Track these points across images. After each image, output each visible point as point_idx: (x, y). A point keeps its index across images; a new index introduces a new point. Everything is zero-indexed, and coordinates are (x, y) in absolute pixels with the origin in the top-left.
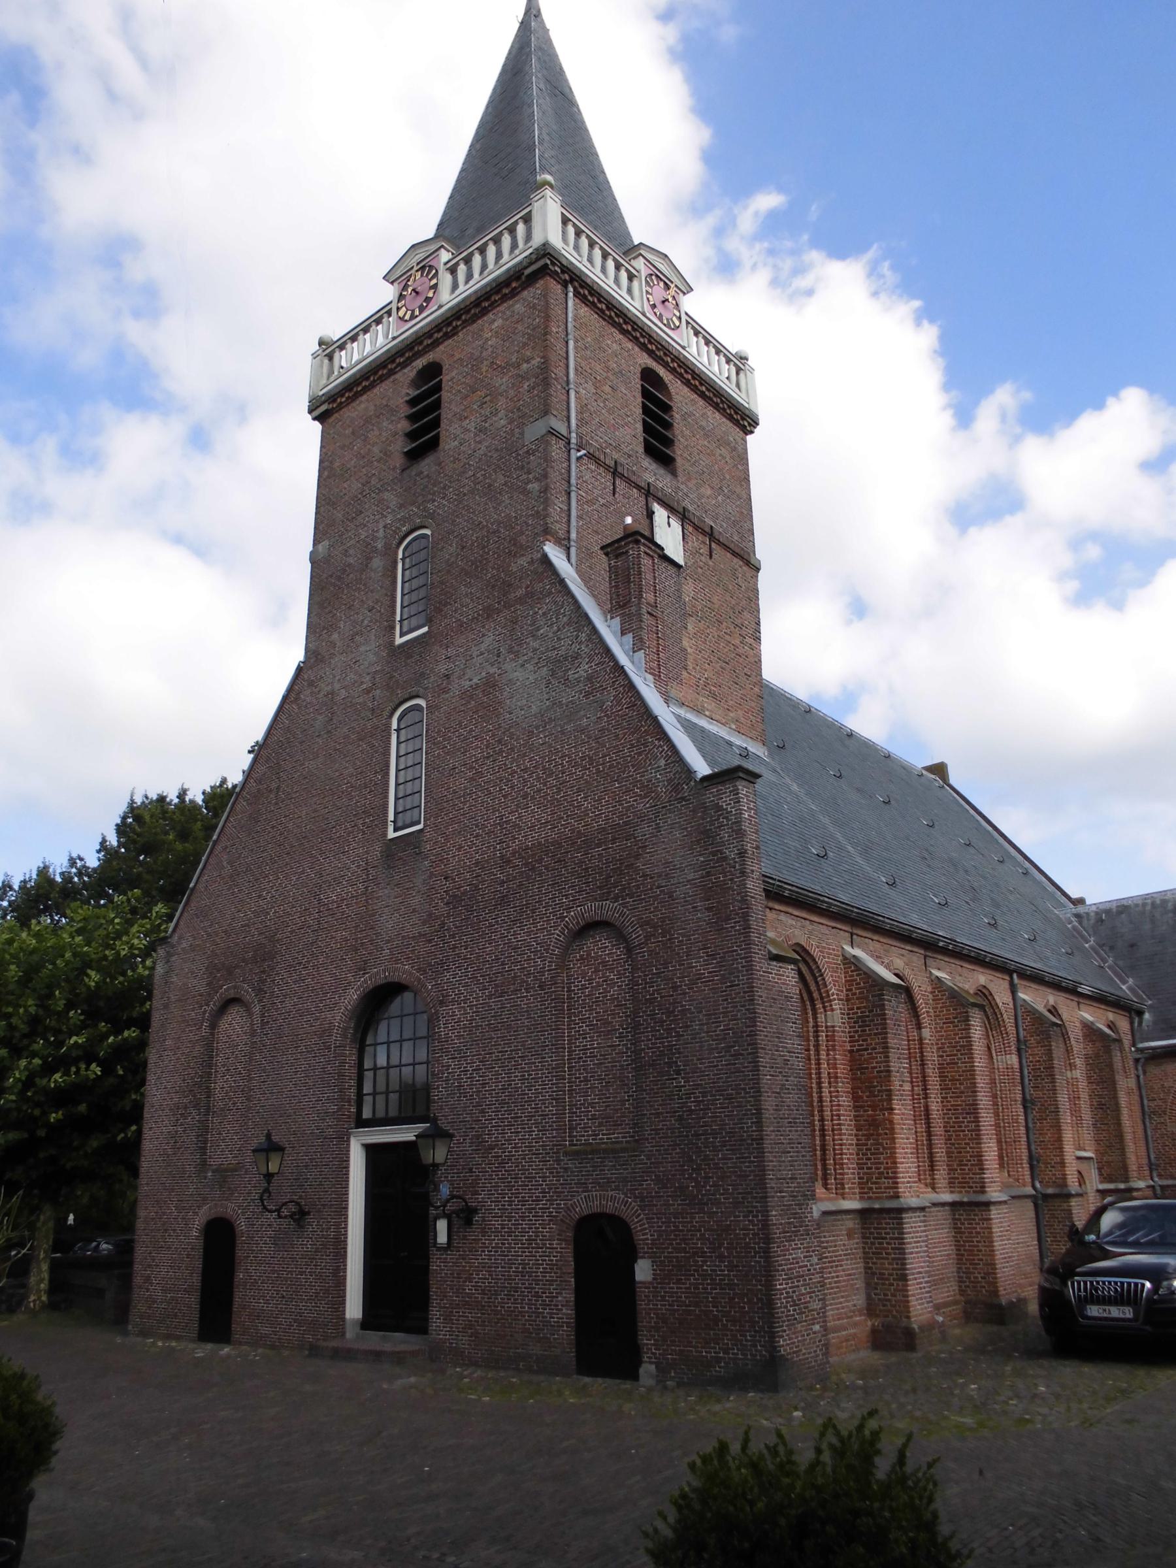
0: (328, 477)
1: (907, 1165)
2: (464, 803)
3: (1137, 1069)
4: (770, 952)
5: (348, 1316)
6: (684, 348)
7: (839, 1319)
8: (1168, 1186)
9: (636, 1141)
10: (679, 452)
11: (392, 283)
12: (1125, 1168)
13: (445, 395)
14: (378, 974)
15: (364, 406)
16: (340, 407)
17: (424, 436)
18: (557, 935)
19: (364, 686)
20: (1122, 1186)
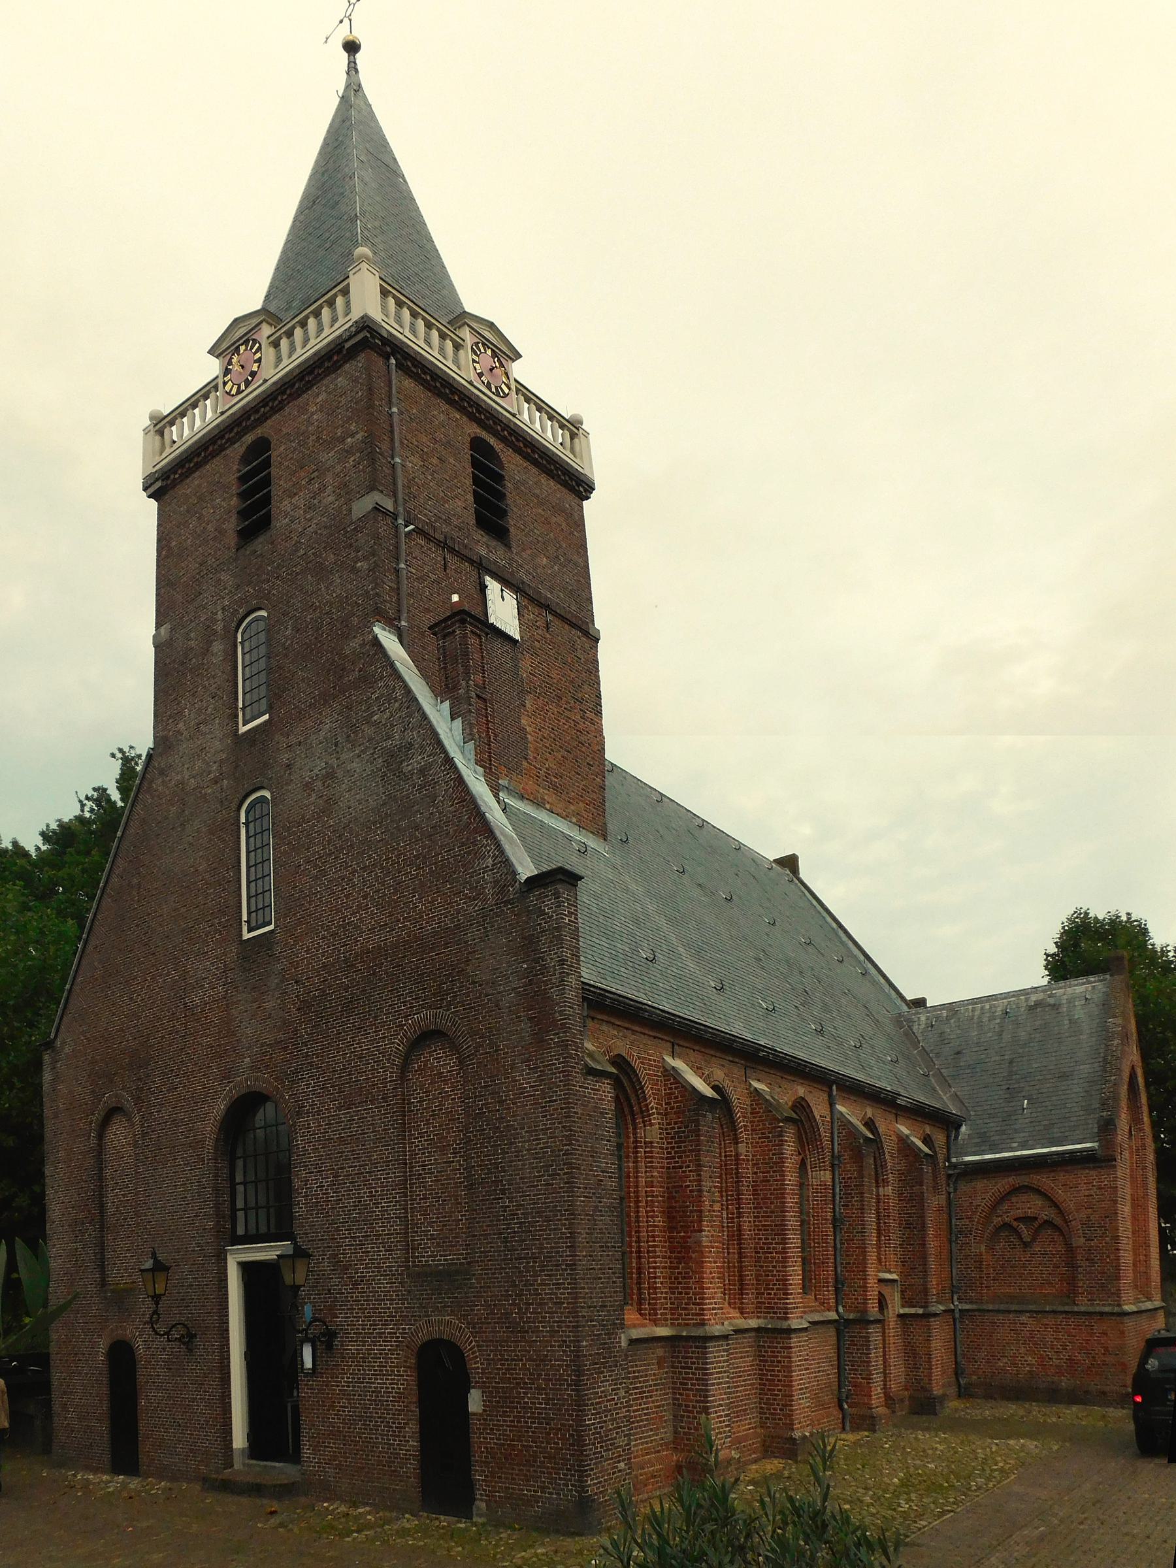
0: (167, 557)
1: (714, 1291)
2: (310, 903)
3: (948, 1185)
4: (586, 1065)
5: (235, 1446)
6: (514, 415)
7: (647, 1454)
8: (968, 1310)
9: (469, 1263)
10: (513, 523)
11: (217, 357)
12: (925, 1291)
13: (274, 471)
14: (244, 1080)
15: (197, 482)
16: (174, 485)
17: (255, 517)
18: (397, 1045)
19: (212, 776)
20: (920, 1311)
